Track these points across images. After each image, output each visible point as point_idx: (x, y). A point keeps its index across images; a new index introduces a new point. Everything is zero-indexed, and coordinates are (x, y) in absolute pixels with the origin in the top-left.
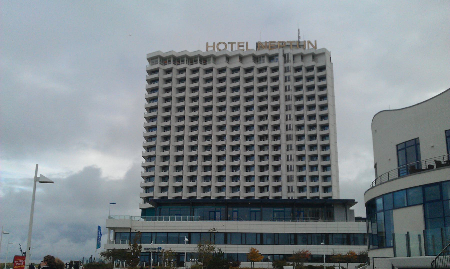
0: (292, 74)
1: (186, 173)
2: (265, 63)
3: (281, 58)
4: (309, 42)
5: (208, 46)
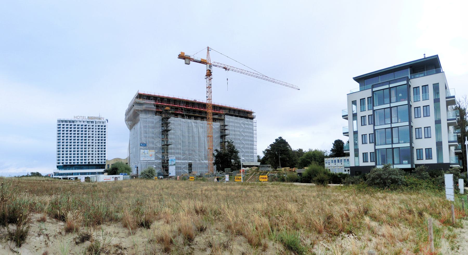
0: (97, 127)
1: (84, 135)
3: (94, 123)
4: (102, 118)
5: (74, 117)
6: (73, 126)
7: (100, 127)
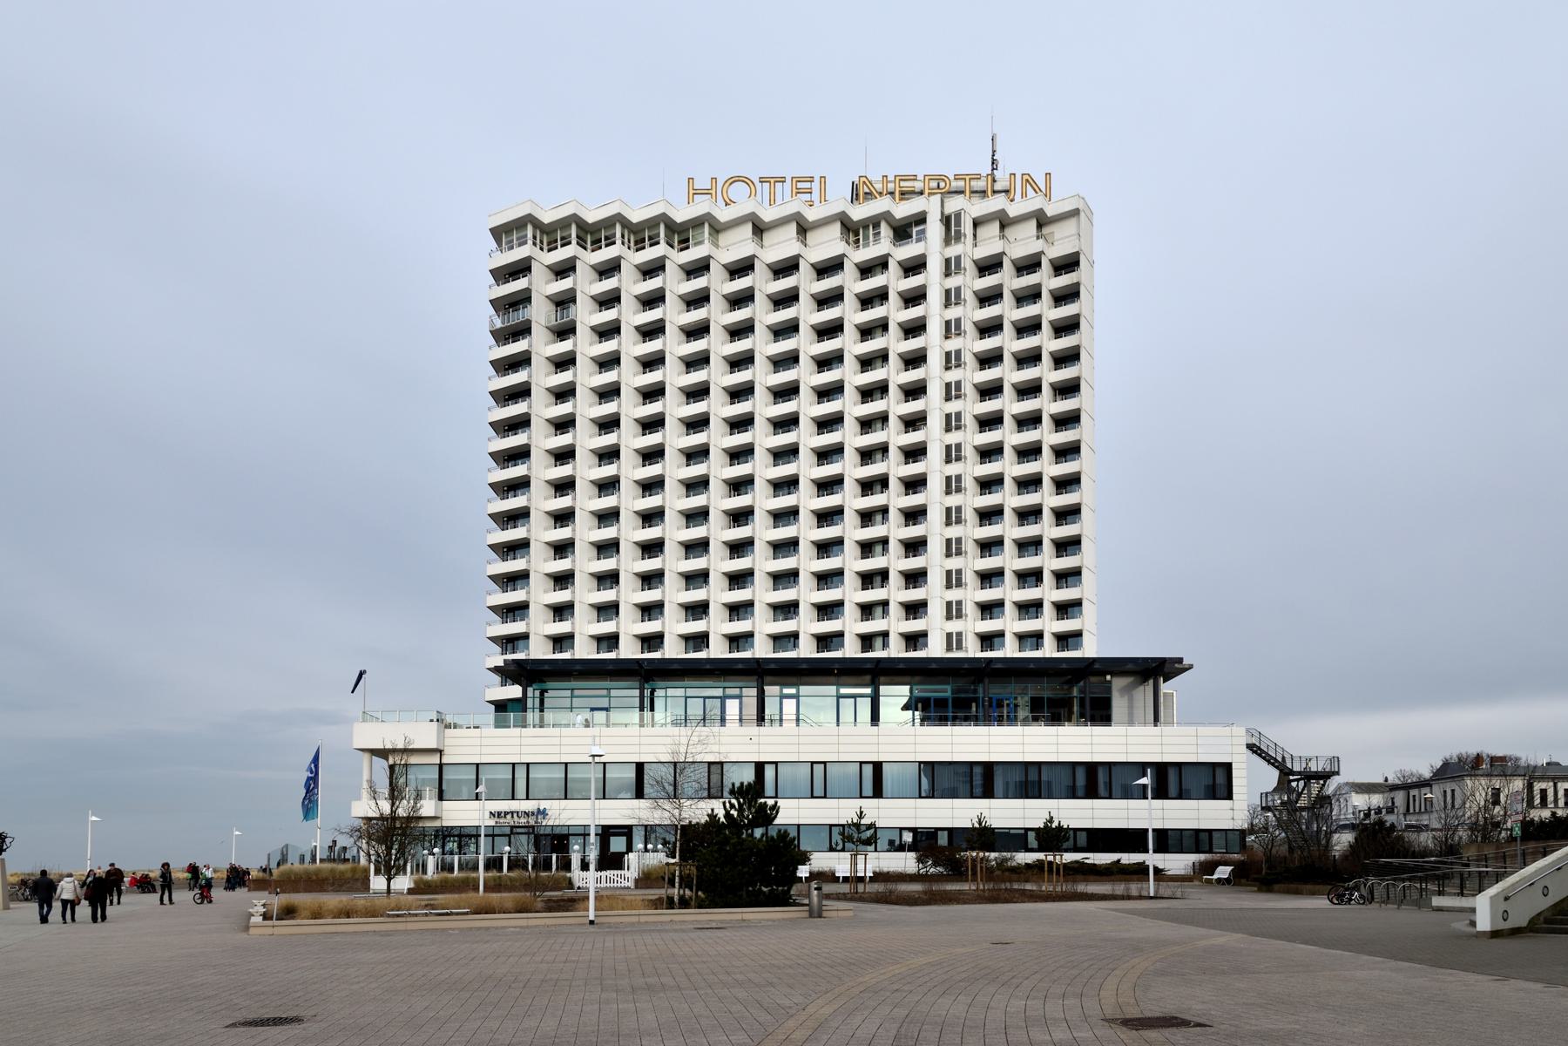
2: (882, 245)
3: (934, 229)
6: (676, 285)
7: (1008, 280)
